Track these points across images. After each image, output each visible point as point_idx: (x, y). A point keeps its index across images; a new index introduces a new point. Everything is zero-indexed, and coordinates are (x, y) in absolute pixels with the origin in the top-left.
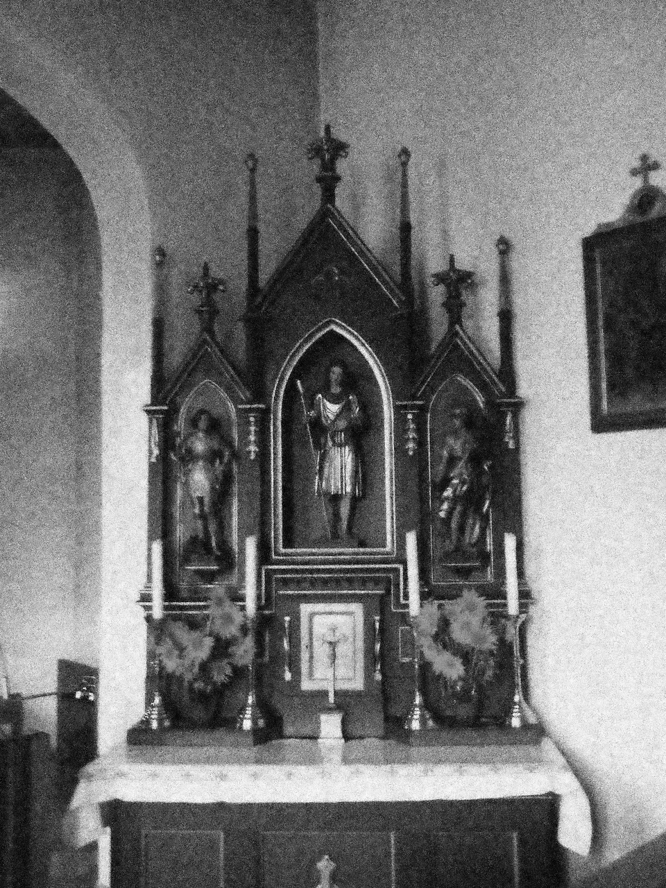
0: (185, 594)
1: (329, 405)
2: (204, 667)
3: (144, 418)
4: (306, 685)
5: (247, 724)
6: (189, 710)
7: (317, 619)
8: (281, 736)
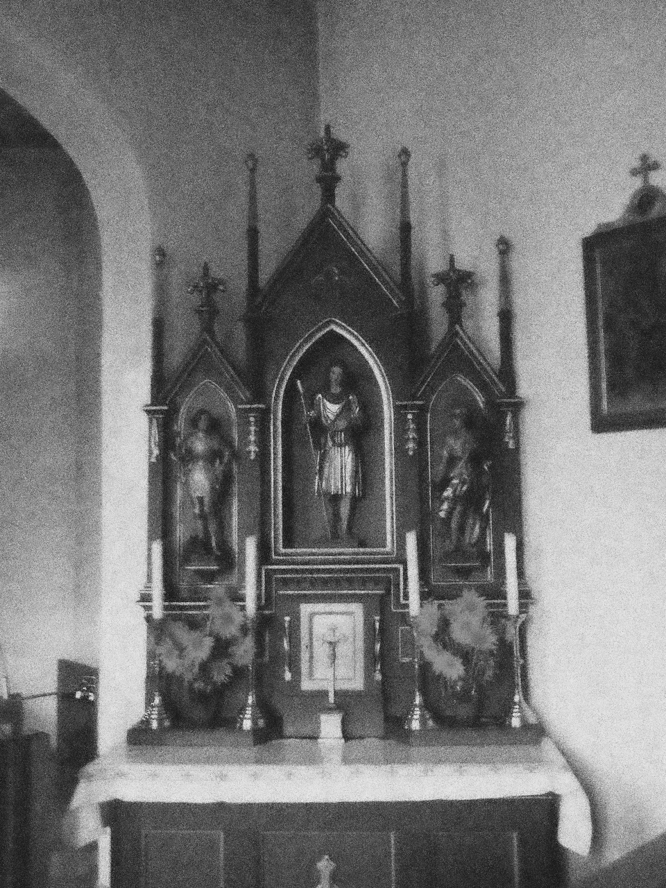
0: (185, 594)
1: (329, 405)
2: (205, 668)
3: (144, 418)
4: (306, 685)
5: (247, 724)
6: (189, 710)
7: (316, 619)
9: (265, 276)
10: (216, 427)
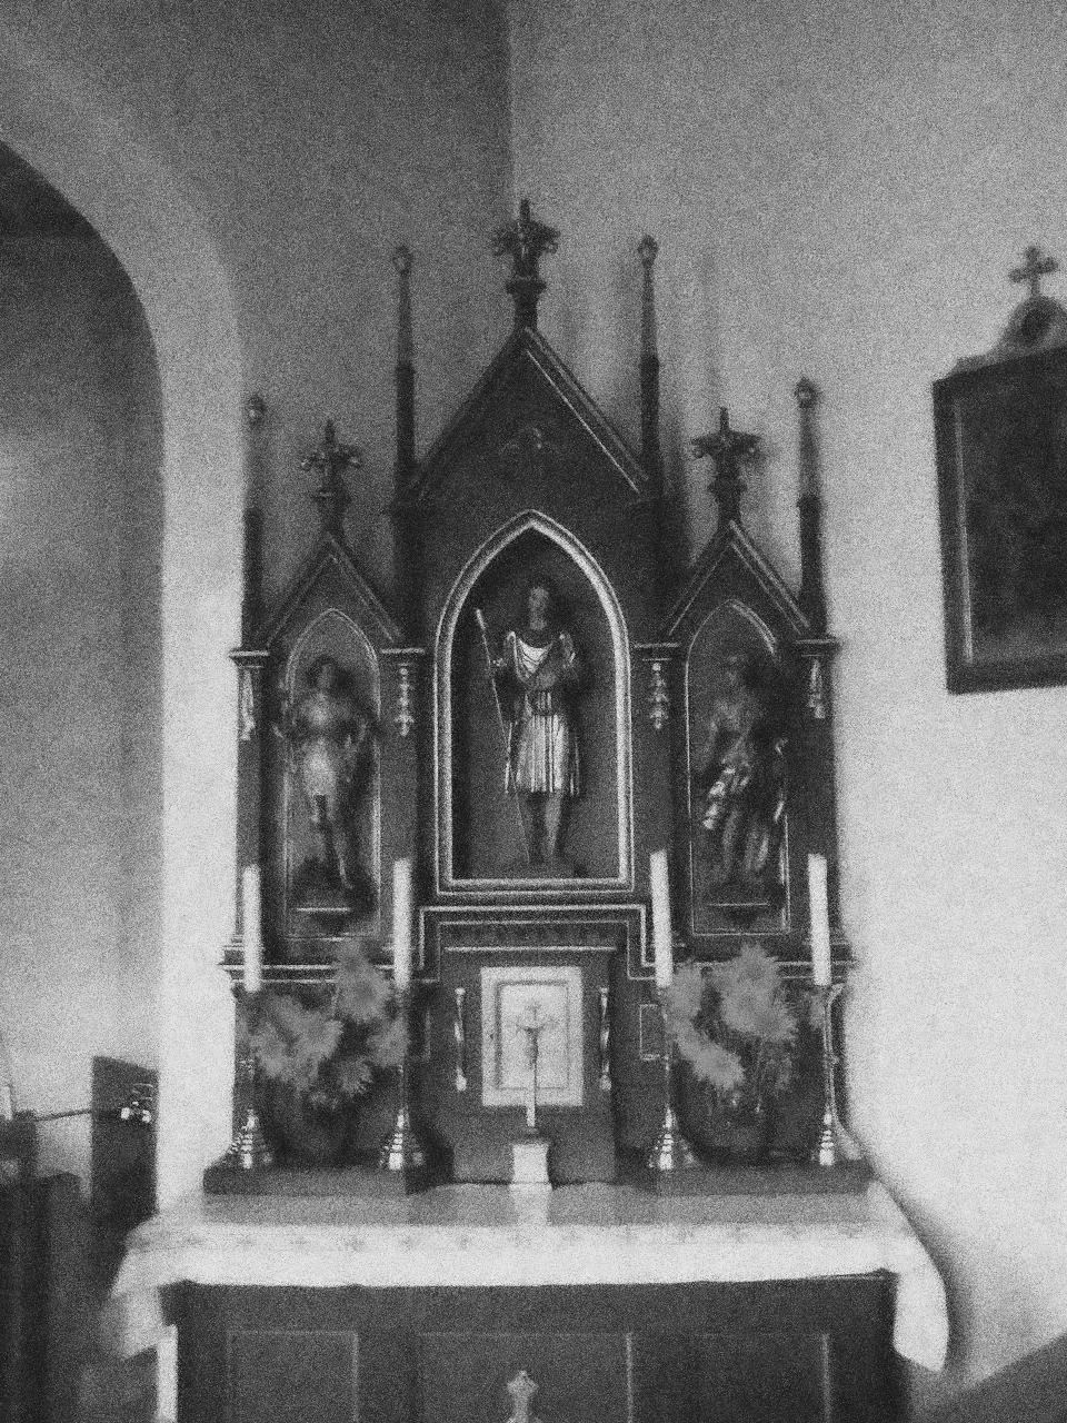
1: (526, 649)
2: (328, 1070)
3: (231, 670)
4: (491, 1098)
5: (396, 1161)
6: (303, 1137)
7: (507, 992)
8: (450, 1179)
9: (424, 442)
10: (346, 684)
